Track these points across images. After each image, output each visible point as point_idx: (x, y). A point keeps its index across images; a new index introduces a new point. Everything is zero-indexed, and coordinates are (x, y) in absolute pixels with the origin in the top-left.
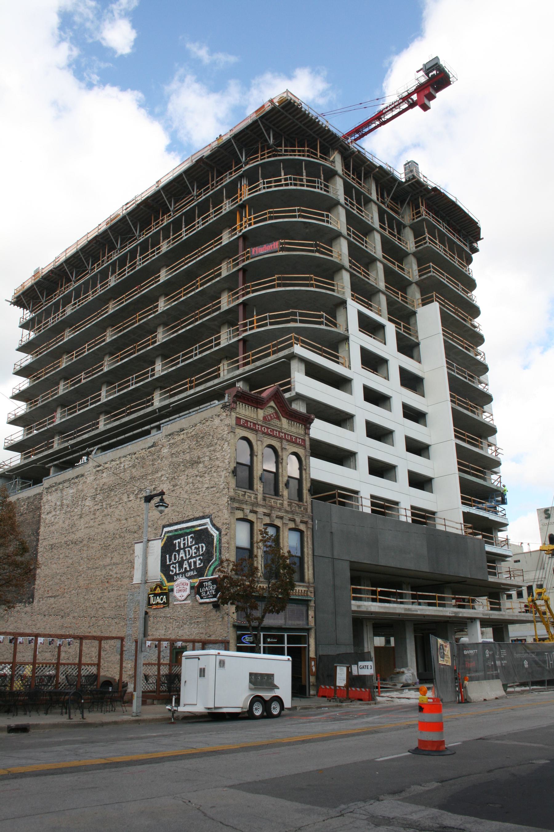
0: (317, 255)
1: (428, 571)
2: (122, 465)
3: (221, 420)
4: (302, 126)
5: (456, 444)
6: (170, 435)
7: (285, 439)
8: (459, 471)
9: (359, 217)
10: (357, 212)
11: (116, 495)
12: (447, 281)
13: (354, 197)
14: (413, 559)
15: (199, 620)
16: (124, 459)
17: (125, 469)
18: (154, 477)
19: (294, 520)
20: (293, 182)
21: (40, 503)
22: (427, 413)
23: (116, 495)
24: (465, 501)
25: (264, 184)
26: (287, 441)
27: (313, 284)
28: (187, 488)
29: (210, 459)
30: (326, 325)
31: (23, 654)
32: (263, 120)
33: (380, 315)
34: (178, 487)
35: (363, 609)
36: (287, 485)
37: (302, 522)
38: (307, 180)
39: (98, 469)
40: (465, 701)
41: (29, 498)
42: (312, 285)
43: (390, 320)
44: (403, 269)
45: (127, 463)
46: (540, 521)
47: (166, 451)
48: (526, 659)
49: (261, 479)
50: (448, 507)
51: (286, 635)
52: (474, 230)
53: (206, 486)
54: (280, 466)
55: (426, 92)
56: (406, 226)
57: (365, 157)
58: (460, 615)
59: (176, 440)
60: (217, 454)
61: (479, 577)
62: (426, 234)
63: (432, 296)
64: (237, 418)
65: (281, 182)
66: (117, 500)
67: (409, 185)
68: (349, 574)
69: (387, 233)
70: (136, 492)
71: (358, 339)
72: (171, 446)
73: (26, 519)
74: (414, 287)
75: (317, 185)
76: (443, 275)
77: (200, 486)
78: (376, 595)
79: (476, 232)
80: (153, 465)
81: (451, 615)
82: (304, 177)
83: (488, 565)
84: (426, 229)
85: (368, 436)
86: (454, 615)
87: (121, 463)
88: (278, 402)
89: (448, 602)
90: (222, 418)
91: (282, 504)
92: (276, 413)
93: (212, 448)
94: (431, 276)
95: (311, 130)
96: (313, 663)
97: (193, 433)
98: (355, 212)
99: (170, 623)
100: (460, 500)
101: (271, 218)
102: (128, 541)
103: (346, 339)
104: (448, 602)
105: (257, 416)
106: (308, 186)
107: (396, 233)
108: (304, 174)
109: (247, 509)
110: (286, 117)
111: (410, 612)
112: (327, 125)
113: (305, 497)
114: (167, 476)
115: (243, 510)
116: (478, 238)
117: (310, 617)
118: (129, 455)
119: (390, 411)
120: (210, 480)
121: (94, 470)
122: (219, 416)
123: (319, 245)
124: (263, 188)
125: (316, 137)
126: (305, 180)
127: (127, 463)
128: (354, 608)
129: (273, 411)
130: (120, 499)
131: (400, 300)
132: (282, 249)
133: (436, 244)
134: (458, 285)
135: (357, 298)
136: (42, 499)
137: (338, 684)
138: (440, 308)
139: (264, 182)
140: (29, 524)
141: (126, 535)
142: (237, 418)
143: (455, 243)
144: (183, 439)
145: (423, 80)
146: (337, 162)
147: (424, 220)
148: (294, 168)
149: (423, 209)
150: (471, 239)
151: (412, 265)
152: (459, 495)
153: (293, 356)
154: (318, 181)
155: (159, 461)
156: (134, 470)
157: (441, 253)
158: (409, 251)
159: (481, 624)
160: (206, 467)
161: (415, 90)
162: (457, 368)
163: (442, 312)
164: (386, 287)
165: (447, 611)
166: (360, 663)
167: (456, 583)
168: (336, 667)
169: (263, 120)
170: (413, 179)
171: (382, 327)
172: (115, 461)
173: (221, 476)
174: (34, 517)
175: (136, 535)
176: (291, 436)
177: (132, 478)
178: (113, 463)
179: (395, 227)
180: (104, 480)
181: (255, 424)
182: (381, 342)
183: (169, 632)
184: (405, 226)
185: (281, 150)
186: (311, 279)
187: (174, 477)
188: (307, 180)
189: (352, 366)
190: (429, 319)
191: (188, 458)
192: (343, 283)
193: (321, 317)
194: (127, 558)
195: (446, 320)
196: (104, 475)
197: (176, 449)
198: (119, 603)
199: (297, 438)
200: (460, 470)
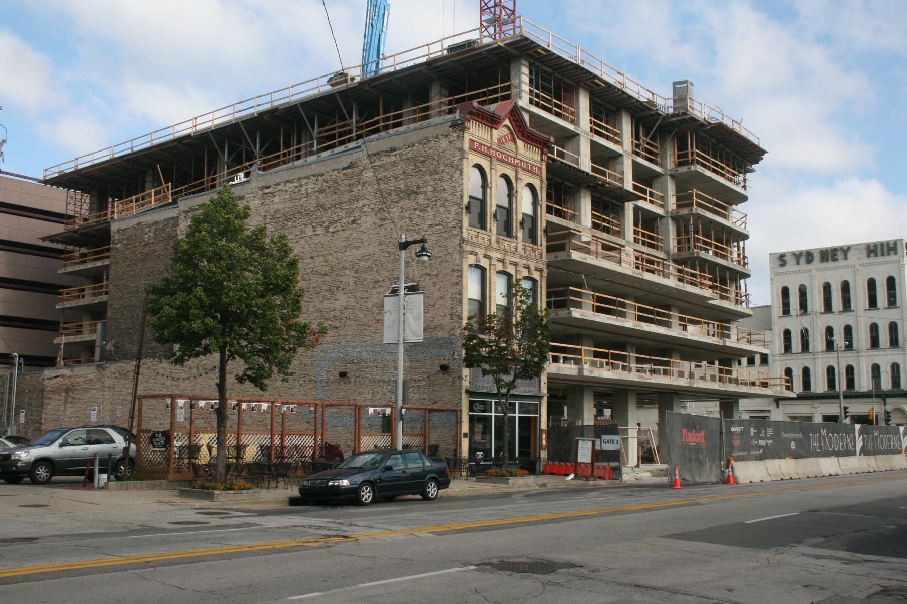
2: (303, 189)
3: (450, 142)
6: (375, 155)
11: (295, 227)
15: (421, 383)
16: (305, 181)
17: (307, 194)
18: (353, 206)
19: (528, 268)
21: (176, 230)
23: (295, 227)
26: (523, 169)
28: (402, 223)
29: (435, 189)
31: (162, 421)
34: (387, 222)
36: (521, 224)
37: (536, 269)
39: (266, 191)
40: (727, 481)
41: (156, 223)
45: (311, 186)
46: (772, 269)
47: (369, 174)
48: (794, 439)
49: (495, 216)
51: (517, 402)
53: (429, 223)
59: (385, 162)
60: (445, 184)
64: (470, 140)
66: (297, 233)
70: (326, 224)
72: (375, 169)
73: (154, 251)
77: (420, 222)
80: (351, 191)
87: (301, 186)
90: (452, 139)
93: (437, 177)
96: (544, 436)
97: (409, 155)
99: (380, 386)
102: (315, 285)
105: (491, 138)
109: (481, 252)
114: (372, 206)
115: (476, 254)
118: (314, 176)
120: (434, 216)
121: (260, 193)
122: (446, 136)
127: (311, 186)
130: (302, 232)
136: (178, 225)
137: (580, 460)
140: (159, 256)
141: (312, 277)
142: (470, 140)
144: (394, 162)
155: (360, 187)
156: (321, 197)
160: (428, 200)
166: (604, 437)
168: (578, 441)
172: (291, 182)
173: (450, 212)
174: (166, 249)
175: (327, 278)
177: (320, 206)
178: (290, 185)
180: (277, 207)
181: (489, 148)
183: (379, 397)
187: (382, 209)
191: (402, 187)
194: (315, 306)
196: (276, 199)
197: (385, 174)
198: (304, 361)
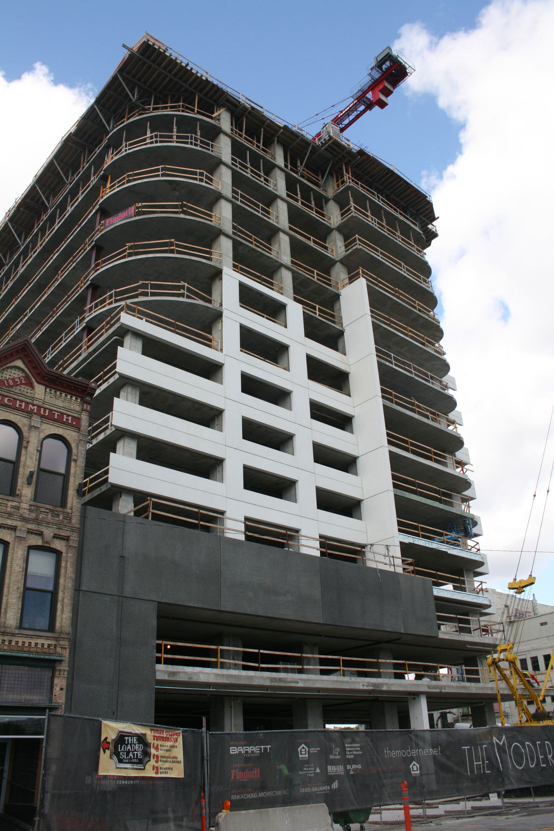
0: (182, 216)
1: (322, 622)
4: (172, 77)
5: (390, 452)
7: (38, 413)
8: (394, 487)
9: (253, 180)
10: (251, 175)
12: (382, 258)
13: (248, 160)
14: (298, 604)
20: (158, 139)
22: (354, 416)
24: (403, 527)
25: (126, 147)
27: (174, 249)
30: (188, 297)
32: (124, 74)
33: (282, 294)
35: (182, 678)
37: (56, 537)
38: (177, 136)
42: (172, 251)
43: (296, 300)
44: (326, 248)
50: (380, 534)
52: (424, 206)
54: (23, 452)
55: (381, 87)
56: (329, 200)
57: (263, 116)
58: (385, 688)
61: (422, 631)
62: (352, 204)
63: (358, 273)
65: (146, 141)
67: (326, 149)
68: (155, 622)
69: (300, 204)
71: (235, 316)
74: (338, 265)
75: (189, 141)
76: (377, 251)
78: (217, 657)
79: (427, 209)
81: (365, 688)
82: (175, 133)
83: (438, 616)
84: (351, 199)
85: (244, 438)
86: (371, 688)
88: (30, 361)
89: (385, 671)
91: (18, 508)
92: (27, 377)
94: (357, 249)
95: (185, 82)
98: (249, 176)
100: (396, 527)
101: (129, 181)
103: (219, 315)
104: (385, 671)
106: (177, 142)
107: (313, 206)
108: (175, 130)
110: (150, 66)
111: (282, 684)
112: (207, 76)
113: (70, 500)
116: (432, 218)
117: (57, 689)
119: (291, 409)
123: (185, 206)
124: (126, 150)
125: (194, 91)
126: (175, 137)
128: (160, 676)
129: (21, 374)
131: (315, 280)
132: (138, 214)
133: (367, 216)
134: (400, 265)
135: (242, 269)
138: (367, 285)
139: (126, 145)
143: (396, 218)
145: (377, 75)
146: (224, 120)
147: (348, 188)
148: (162, 125)
149: (346, 176)
150: (424, 219)
151: (336, 242)
152: (394, 519)
153: (125, 331)
154: (192, 137)
157: (374, 226)
158: (332, 226)
159: (428, 702)
161: (369, 87)
162: (395, 359)
163: (371, 292)
164: (293, 262)
165: (358, 683)
167: (388, 642)
169: (124, 74)
170: (329, 140)
171: (282, 307)
176: (51, 410)
179: (312, 199)
182: (281, 325)
184: (327, 200)
185: (150, 108)
186: (172, 244)
188: (177, 136)
189: (224, 349)
190: (355, 301)
192: (220, 250)
193: (183, 287)
195: (376, 301)
199: (63, 414)
200: (395, 486)
